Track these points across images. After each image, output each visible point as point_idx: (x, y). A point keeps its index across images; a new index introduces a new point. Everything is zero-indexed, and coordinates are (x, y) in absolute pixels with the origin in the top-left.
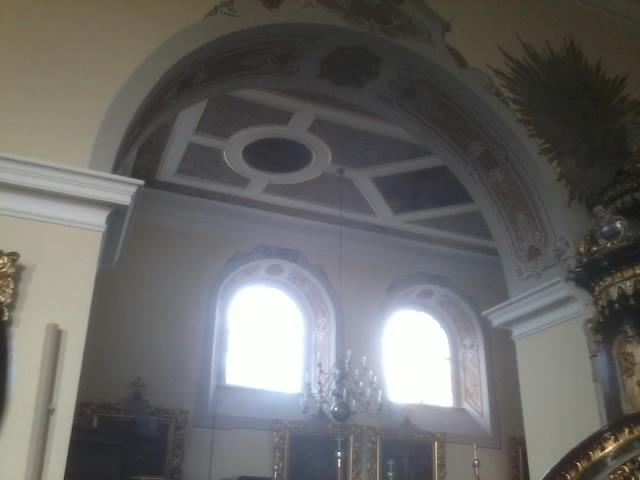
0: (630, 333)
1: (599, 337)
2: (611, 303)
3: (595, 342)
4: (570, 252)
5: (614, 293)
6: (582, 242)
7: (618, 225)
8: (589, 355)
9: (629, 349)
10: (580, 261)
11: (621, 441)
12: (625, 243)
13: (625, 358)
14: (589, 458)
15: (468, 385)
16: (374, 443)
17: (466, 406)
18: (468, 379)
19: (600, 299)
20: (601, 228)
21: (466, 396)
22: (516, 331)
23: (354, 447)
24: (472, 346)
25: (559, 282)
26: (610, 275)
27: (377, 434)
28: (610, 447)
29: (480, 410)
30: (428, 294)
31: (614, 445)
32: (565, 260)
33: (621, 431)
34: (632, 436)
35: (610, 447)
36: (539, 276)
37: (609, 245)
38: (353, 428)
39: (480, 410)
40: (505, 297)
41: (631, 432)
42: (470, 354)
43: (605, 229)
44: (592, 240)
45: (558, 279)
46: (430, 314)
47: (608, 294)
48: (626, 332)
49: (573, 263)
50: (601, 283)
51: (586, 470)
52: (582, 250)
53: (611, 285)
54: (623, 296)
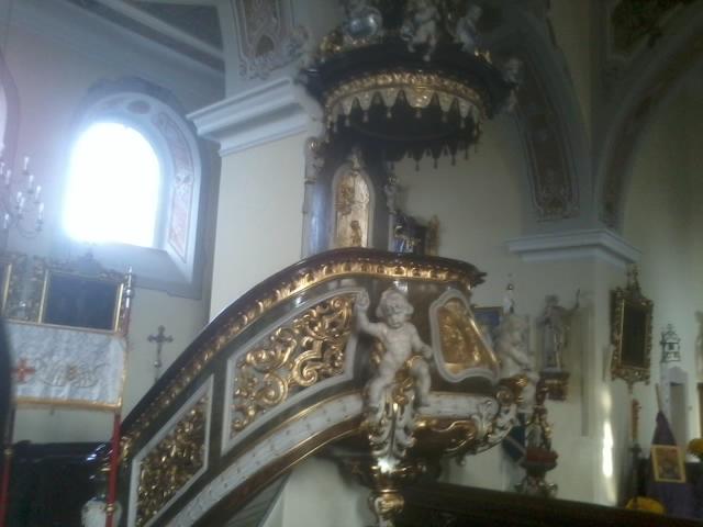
0: (357, 165)
1: (321, 162)
2: (342, 118)
3: (314, 166)
4: (308, 46)
5: (348, 107)
6: (325, 39)
7: (372, 21)
8: (304, 180)
9: (350, 182)
10: (317, 60)
11: (316, 280)
12: (374, 42)
13: (344, 192)
14: (275, 298)
15: (174, 224)
16: (41, 277)
17: (168, 249)
18: (175, 218)
19: (331, 113)
20: (350, 19)
21: (170, 235)
22: (226, 144)
23: (11, 280)
24: (187, 180)
25: (286, 83)
26: (348, 81)
27: (45, 267)
28: (303, 285)
29: (183, 255)
30: (140, 107)
31: (308, 284)
32: (300, 55)
33: (318, 268)
34: (330, 275)
35: (303, 285)
36: (265, 78)
37: (355, 43)
38: (14, 256)
39: (183, 255)
40: (222, 97)
41: (329, 271)
42: (183, 189)
43: (355, 23)
44: (337, 37)
45: (364, 238)
46: (137, 129)
47: (342, 109)
48: (353, 163)
49: (307, 60)
50: (337, 92)
51: (268, 311)
52: (323, 47)
53: (344, 97)
54: (357, 111)
